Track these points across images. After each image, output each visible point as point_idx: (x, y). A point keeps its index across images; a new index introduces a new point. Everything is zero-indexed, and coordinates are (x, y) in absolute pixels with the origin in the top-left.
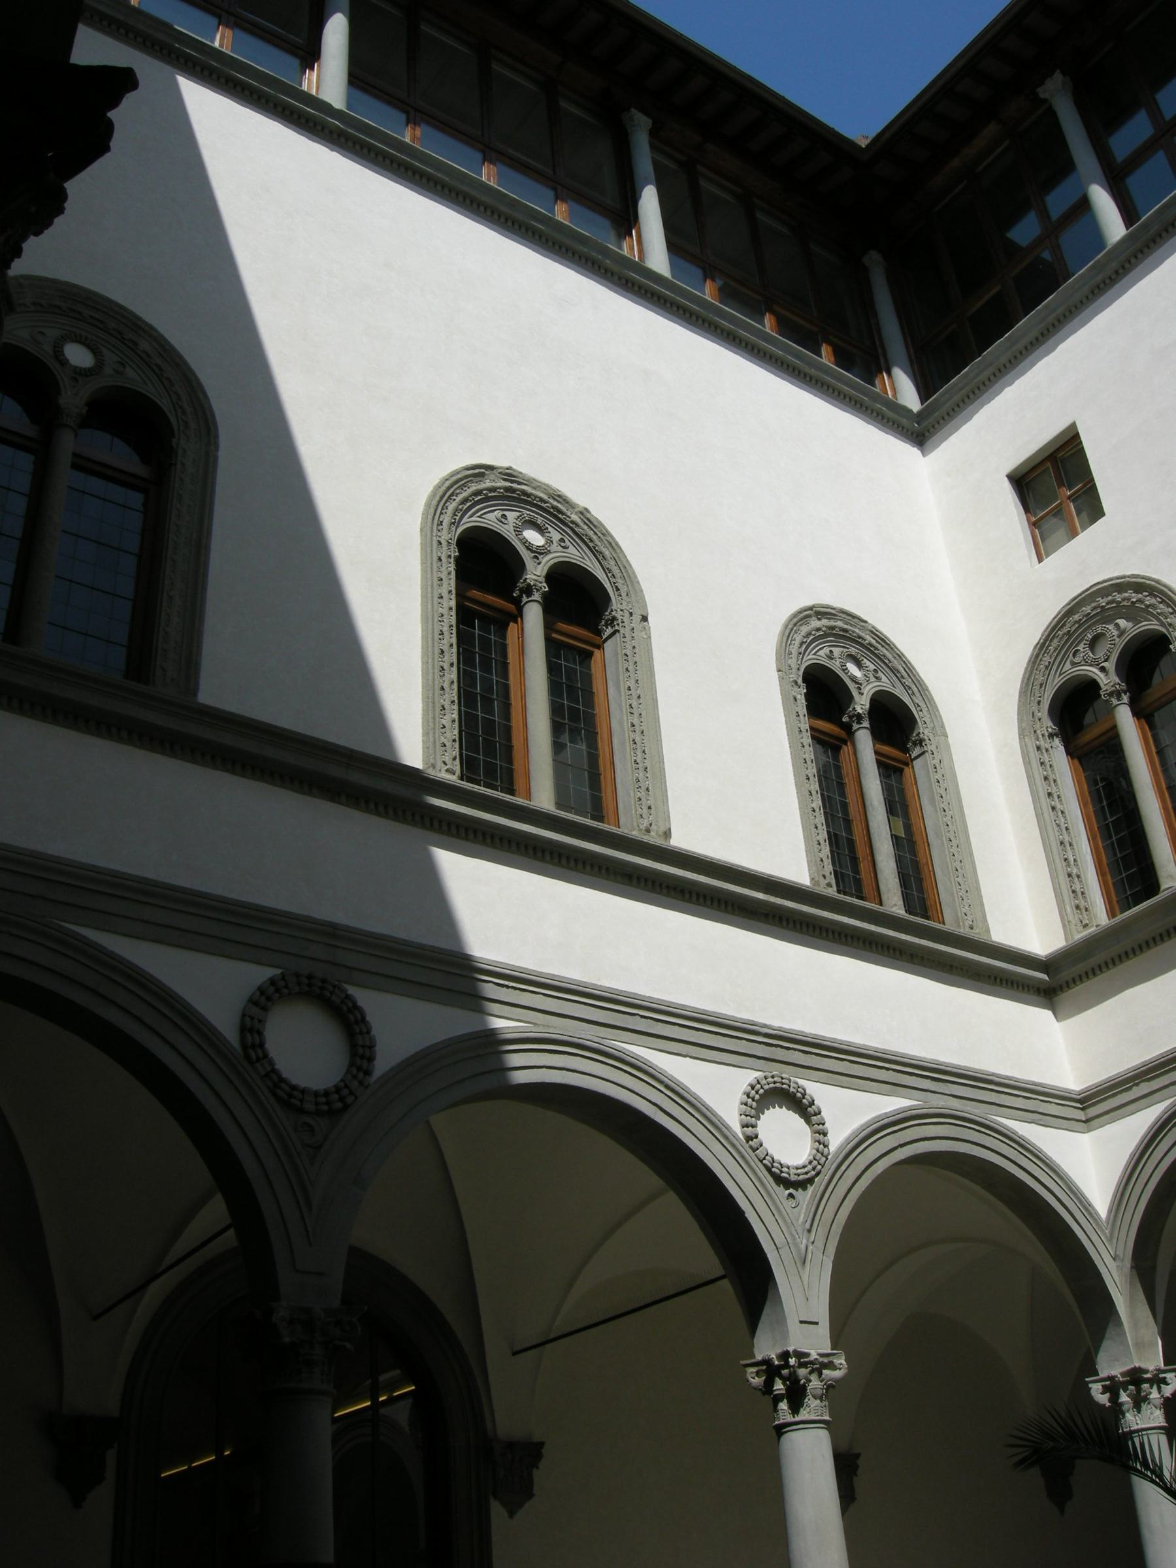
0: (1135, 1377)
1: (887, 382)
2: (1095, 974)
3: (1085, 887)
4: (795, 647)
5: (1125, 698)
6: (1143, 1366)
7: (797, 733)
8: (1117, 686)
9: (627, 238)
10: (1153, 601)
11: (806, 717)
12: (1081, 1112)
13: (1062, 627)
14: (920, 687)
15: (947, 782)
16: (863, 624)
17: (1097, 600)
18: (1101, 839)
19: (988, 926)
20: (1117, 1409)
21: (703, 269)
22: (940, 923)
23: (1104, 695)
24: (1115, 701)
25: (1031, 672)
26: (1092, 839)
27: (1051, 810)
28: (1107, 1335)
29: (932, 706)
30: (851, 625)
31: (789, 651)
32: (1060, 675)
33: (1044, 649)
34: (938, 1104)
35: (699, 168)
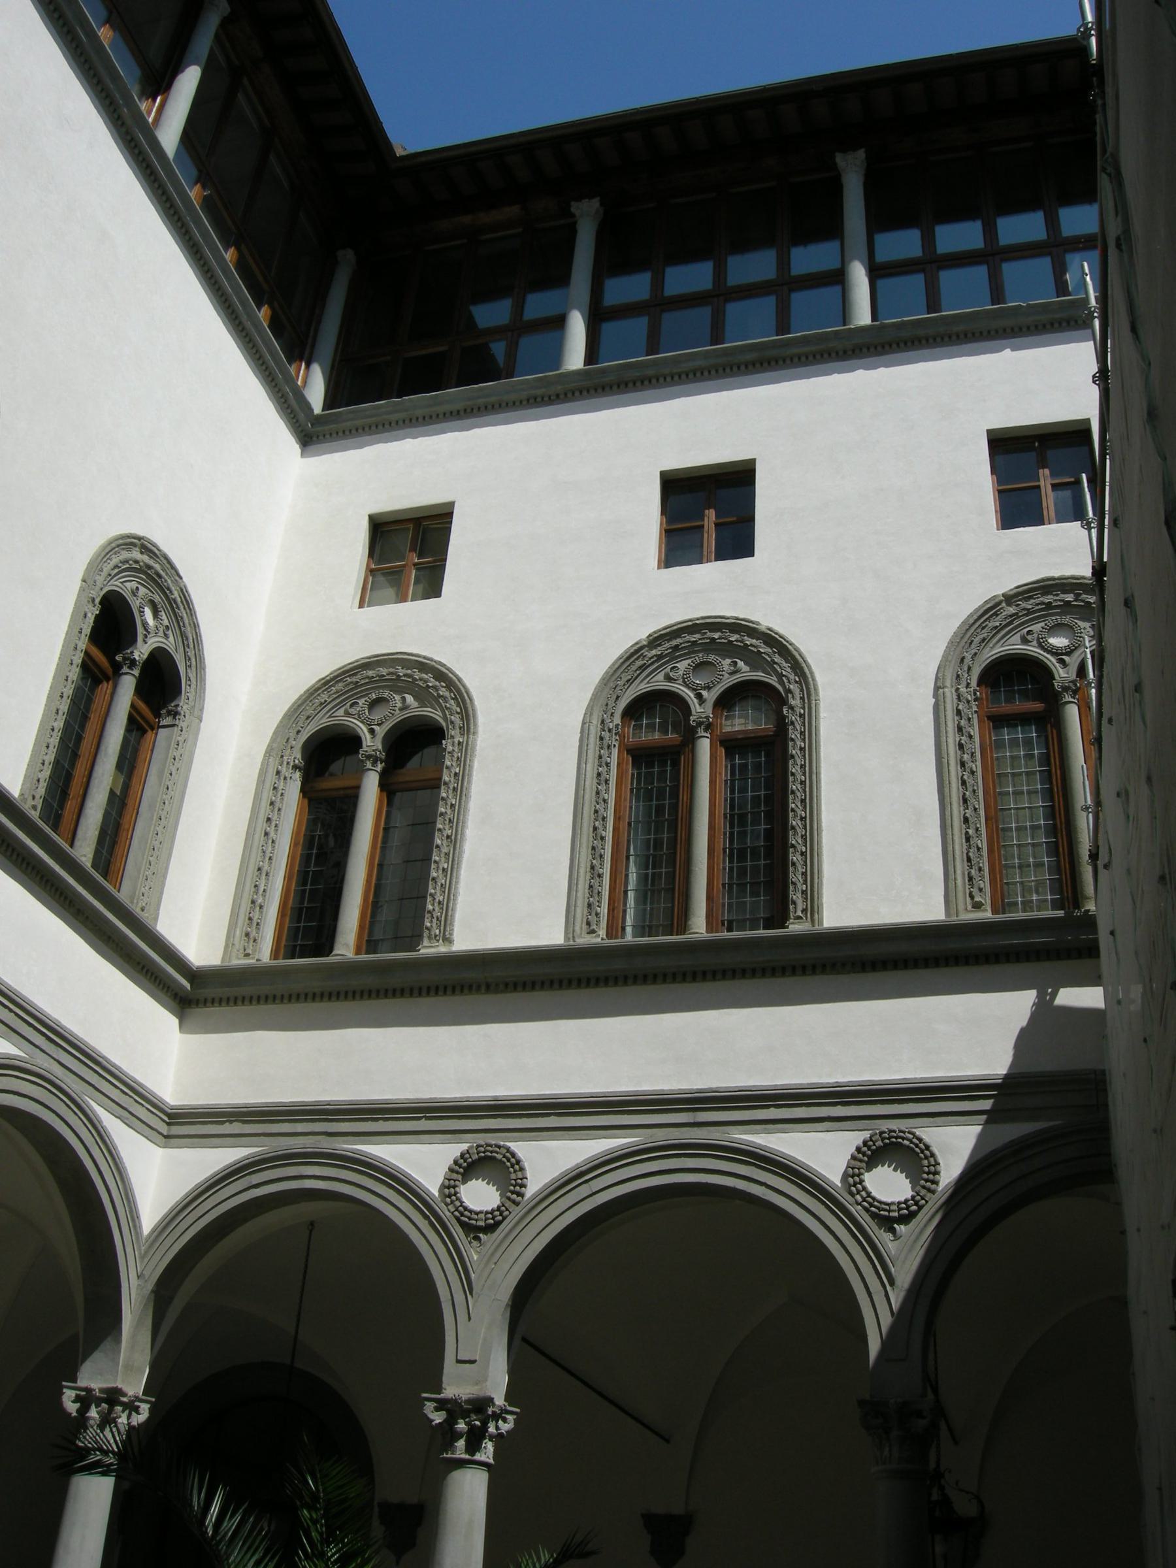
0: (112, 1397)
1: (302, 372)
2: (235, 1004)
3: (263, 920)
4: (108, 566)
5: (379, 767)
6: (125, 1389)
7: (72, 648)
8: (378, 753)
9: (150, 100)
10: (447, 694)
11: (87, 638)
12: (166, 1127)
13: (353, 675)
14: (198, 663)
15: (181, 764)
16: (177, 578)
17: (397, 667)
18: (296, 883)
19: (158, 915)
20: (81, 1421)
21: (200, 171)
22: (115, 888)
23: (363, 754)
24: (369, 765)
25: (305, 701)
26: (288, 878)
27: (263, 835)
28: (102, 1347)
29: (201, 686)
30: (167, 574)
31: (101, 568)
32: (330, 717)
33: (327, 687)
34: (42, 1064)
35: (245, 81)
